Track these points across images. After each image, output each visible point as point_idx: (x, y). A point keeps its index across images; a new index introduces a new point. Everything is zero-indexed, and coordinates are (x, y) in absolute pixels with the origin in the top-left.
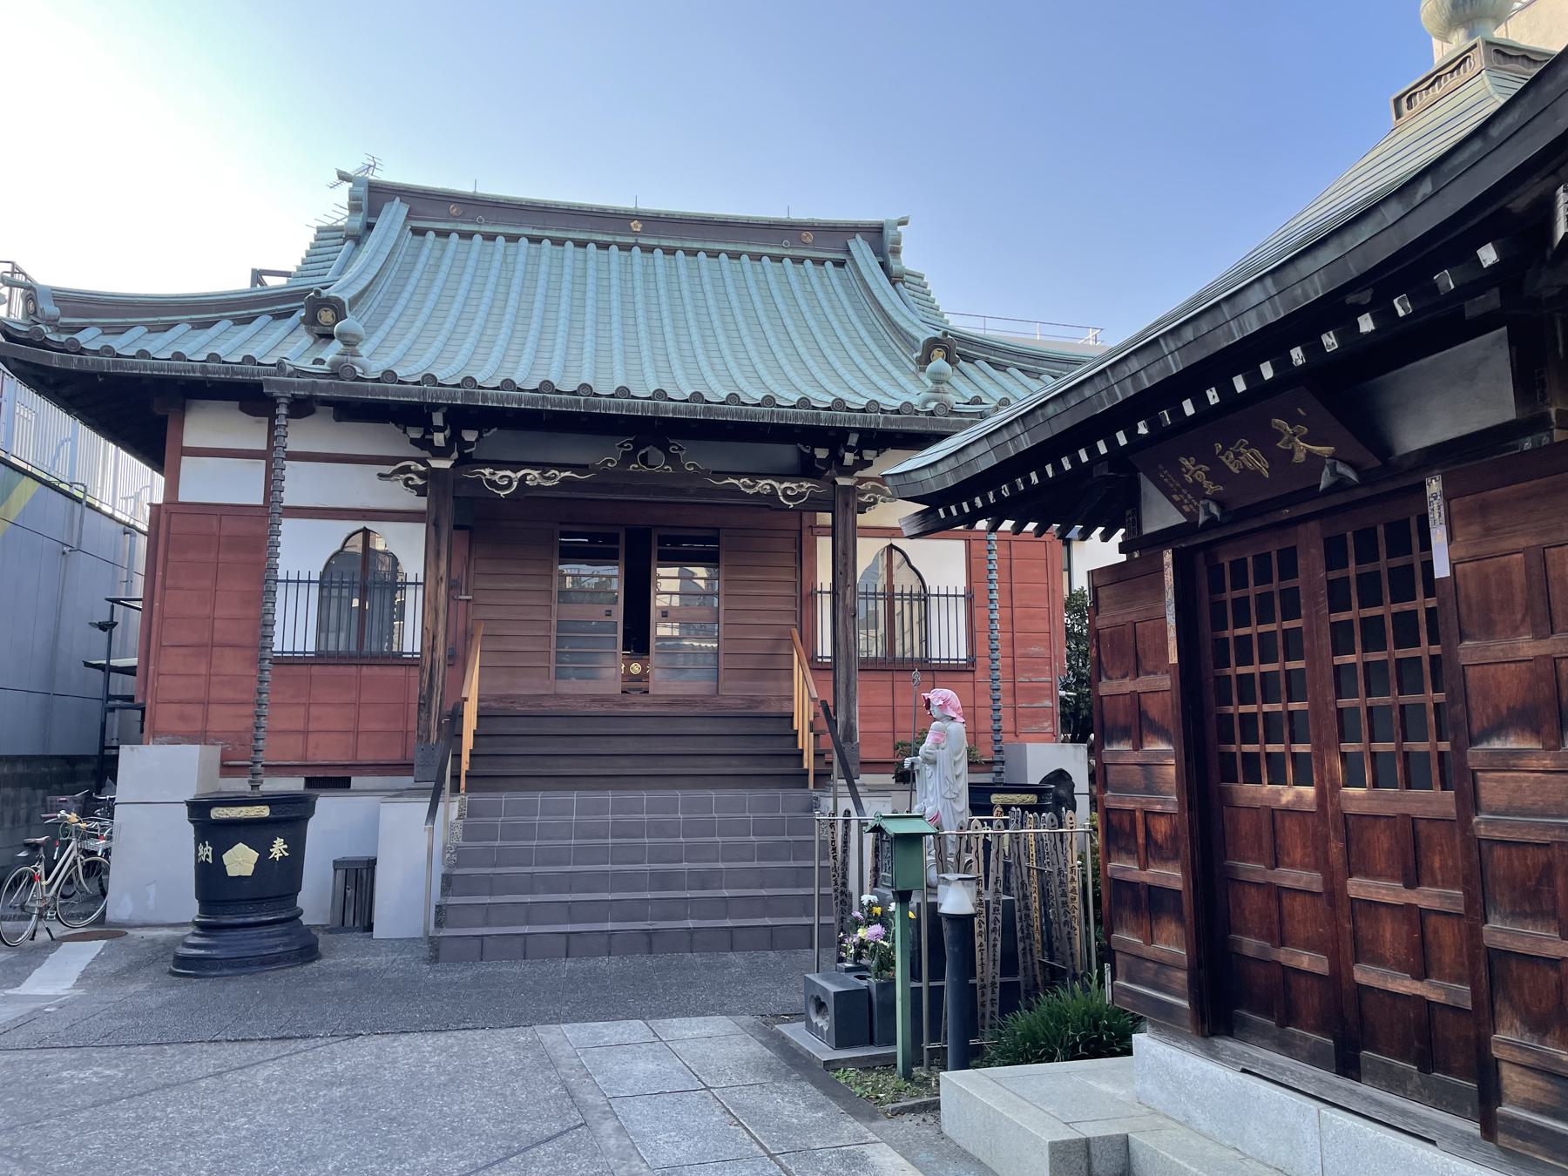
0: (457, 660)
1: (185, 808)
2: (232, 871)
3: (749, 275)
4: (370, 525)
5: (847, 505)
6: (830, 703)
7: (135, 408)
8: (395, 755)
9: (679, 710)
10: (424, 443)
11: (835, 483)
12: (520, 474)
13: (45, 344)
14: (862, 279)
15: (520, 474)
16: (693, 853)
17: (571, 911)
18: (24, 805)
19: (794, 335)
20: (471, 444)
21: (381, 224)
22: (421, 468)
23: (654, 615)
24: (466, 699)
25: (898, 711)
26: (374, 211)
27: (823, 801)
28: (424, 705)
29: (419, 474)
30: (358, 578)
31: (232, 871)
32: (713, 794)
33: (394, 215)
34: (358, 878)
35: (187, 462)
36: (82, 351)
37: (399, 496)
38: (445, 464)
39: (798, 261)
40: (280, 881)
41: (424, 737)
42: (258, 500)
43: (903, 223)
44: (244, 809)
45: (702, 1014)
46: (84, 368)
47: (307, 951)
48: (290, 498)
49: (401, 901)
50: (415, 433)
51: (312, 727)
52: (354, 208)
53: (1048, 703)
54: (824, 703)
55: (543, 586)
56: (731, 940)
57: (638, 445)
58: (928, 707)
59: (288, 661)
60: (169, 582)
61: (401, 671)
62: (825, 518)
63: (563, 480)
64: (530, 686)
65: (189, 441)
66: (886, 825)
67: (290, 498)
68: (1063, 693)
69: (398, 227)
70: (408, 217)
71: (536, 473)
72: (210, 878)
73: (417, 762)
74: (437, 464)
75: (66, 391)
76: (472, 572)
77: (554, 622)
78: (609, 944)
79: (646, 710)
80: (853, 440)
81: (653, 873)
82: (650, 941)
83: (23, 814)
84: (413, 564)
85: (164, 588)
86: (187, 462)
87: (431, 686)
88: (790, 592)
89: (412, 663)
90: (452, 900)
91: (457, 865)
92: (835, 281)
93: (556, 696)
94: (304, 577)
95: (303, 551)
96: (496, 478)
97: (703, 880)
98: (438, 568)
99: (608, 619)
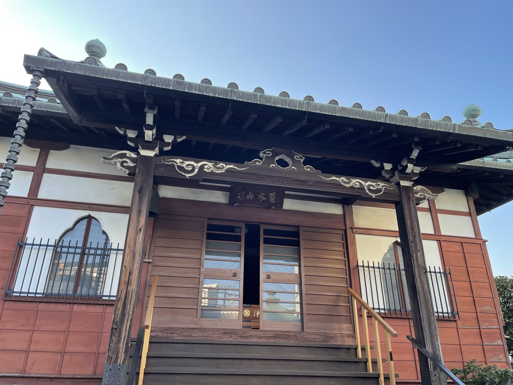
0: (141, 303)
4: (93, 214)
5: (409, 198)
8: (338, 239)
9: (279, 341)
11: (398, 184)
12: (200, 164)
15: (200, 164)
20: (168, 144)
22: (133, 155)
23: (262, 276)
28: (116, 330)
29: (131, 159)
30: (82, 250)
38: (150, 153)
41: (112, 360)
42: (25, 194)
53: (500, 342)
55: (197, 256)
57: (275, 154)
61: (99, 309)
63: (228, 170)
71: (210, 164)
74: (144, 153)
76: (153, 245)
79: (259, 340)
84: (118, 239)
87: (123, 314)
88: (342, 266)
89: (110, 304)
93: (201, 329)
95: (45, 227)
96: (184, 165)
98: (138, 222)
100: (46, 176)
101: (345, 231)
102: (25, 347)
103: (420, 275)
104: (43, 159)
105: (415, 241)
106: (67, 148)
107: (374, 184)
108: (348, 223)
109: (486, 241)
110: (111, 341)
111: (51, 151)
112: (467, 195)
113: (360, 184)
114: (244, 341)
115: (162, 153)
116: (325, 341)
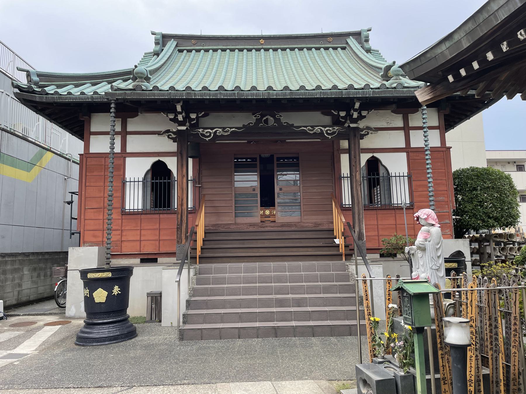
1: (79, 274)
2: (97, 300)
3: (307, 55)
6: (352, 224)
7: (73, 116)
10: (175, 120)
12: (214, 131)
13: (34, 92)
14: (354, 52)
15: (214, 131)
16: (294, 290)
17: (241, 317)
18: (49, 270)
19: (327, 73)
20: (194, 119)
21: (165, 49)
24: (197, 226)
25: (380, 226)
26: (164, 45)
27: (350, 267)
31: (97, 300)
32: (301, 263)
33: (171, 45)
34: (156, 300)
35: (92, 137)
36: (47, 94)
37: (173, 147)
38: (184, 128)
39: (326, 49)
40: (118, 306)
42: (439, 145)
43: (369, 30)
44: (101, 274)
45: (301, 378)
46: (48, 101)
47: (131, 334)
48: (129, 150)
49: (173, 310)
50: (172, 116)
51: (142, 238)
52: (157, 43)
53: (447, 221)
54: (348, 224)
56: (313, 332)
57: (263, 116)
58: (418, 220)
59: (133, 214)
60: (87, 184)
62: (345, 144)
64: (228, 220)
65: (93, 129)
66: (407, 287)
67: (128, 150)
68: (454, 217)
69: (172, 49)
70: (177, 46)
71: (220, 130)
72: (89, 301)
73: (177, 252)
75: (47, 112)
77: (233, 194)
78: (258, 333)
80: (357, 105)
81: (277, 299)
82: (276, 332)
83: (49, 273)
85: (86, 186)
86: (93, 138)
90: (191, 312)
91: (194, 296)
92: (342, 55)
94: (132, 180)
97: (299, 303)
98: (182, 171)
99: (254, 192)
100: (129, 137)
101: (333, 153)
102: (138, 238)
103: (356, 186)
104: (406, 120)
105: (356, 165)
106: (137, 115)
107: (331, 129)
108: (335, 146)
109: (451, 147)
110: (177, 234)
111: (129, 120)
112: (439, 112)
113: (321, 130)
114: (263, 229)
115: (191, 126)
116: (315, 227)
